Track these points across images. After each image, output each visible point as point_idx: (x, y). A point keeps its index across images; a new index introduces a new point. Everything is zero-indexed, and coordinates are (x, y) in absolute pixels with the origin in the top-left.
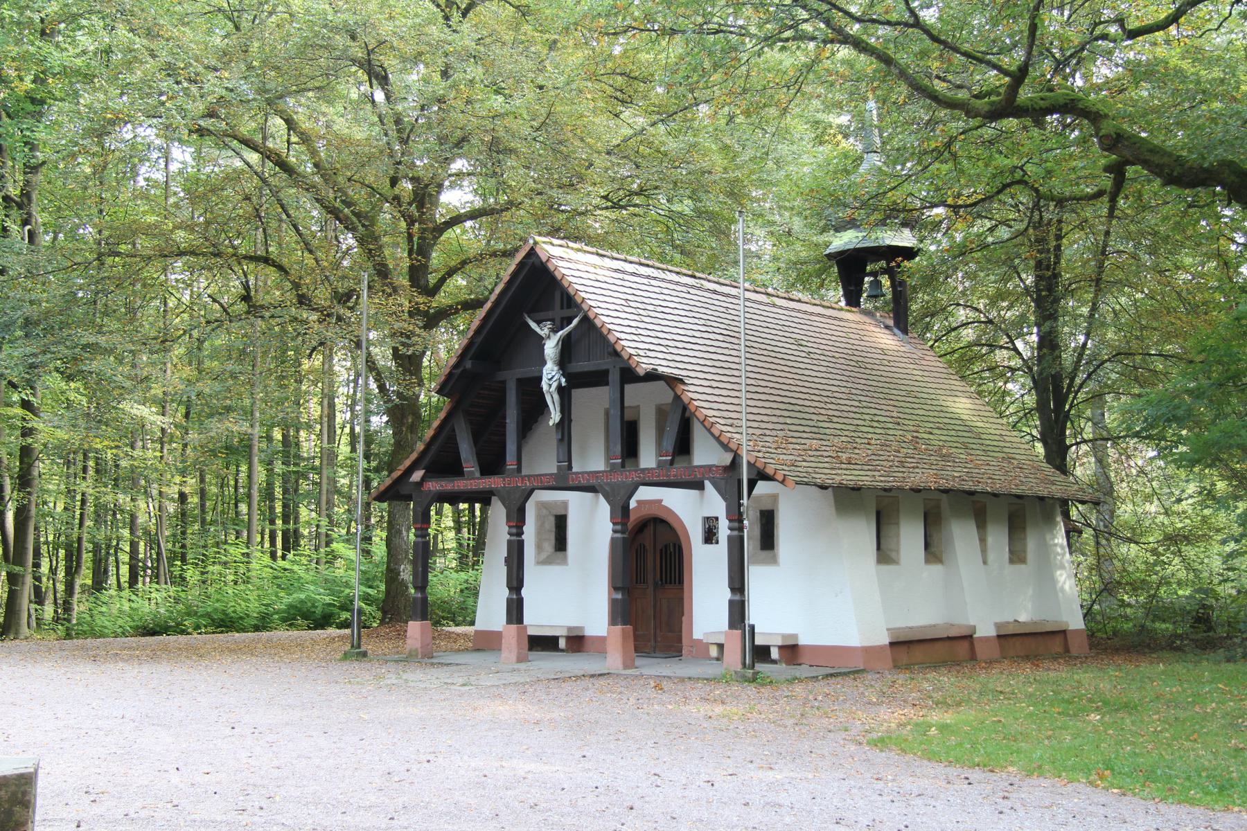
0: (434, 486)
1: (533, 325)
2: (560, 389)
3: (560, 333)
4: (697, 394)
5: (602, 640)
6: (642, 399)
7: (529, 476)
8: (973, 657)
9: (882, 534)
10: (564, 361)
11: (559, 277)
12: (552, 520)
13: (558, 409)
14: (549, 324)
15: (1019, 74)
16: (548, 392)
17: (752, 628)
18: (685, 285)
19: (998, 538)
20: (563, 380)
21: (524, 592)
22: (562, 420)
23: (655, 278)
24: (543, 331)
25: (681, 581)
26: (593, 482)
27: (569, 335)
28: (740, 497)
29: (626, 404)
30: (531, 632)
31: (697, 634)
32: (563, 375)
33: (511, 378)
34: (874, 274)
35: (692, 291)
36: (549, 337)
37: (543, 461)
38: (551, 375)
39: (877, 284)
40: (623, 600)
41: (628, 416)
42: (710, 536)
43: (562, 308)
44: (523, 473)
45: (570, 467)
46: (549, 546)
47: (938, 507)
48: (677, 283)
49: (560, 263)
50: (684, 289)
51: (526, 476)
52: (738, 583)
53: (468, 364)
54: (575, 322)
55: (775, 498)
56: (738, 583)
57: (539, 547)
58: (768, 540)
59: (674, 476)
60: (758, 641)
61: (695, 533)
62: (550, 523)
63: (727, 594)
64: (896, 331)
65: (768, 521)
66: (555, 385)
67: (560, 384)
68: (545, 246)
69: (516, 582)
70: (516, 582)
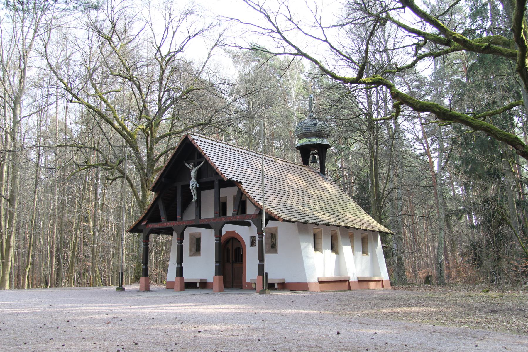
0: (152, 226)
1: (187, 165)
2: (196, 188)
3: (197, 167)
4: (247, 188)
5: (211, 283)
6: (228, 193)
7: (185, 221)
8: (349, 288)
9: (317, 242)
10: (198, 178)
11: (196, 146)
12: (195, 239)
13: (196, 195)
14: (192, 164)
15: (362, 67)
16: (192, 189)
17: (267, 273)
18: (244, 153)
19: (358, 244)
20: (198, 185)
21: (183, 265)
22: (197, 200)
23: (232, 150)
24: (190, 167)
25: (242, 261)
26: (208, 222)
27: (200, 168)
28: (262, 227)
29: (221, 196)
30: (185, 281)
31: (248, 280)
32: (198, 183)
33: (179, 186)
34: (313, 155)
35: (246, 155)
36: (192, 169)
37: (191, 215)
38: (193, 183)
39: (314, 158)
40: (219, 266)
41: (222, 200)
42: (252, 244)
43: (198, 158)
44: (184, 219)
45: (200, 217)
46: (194, 250)
47: (336, 233)
48: (241, 152)
49: (196, 141)
50: (244, 154)
51: (184, 221)
52: (261, 258)
53: (163, 180)
54: (202, 163)
55: (276, 229)
56: (261, 258)
57: (190, 250)
58: (273, 247)
59: (238, 219)
60: (269, 282)
61: (247, 242)
62: (194, 241)
63: (258, 262)
64: (321, 174)
65: (273, 236)
66: (195, 186)
67: (196, 186)
68: (191, 135)
69: (180, 260)
70: (180, 260)
